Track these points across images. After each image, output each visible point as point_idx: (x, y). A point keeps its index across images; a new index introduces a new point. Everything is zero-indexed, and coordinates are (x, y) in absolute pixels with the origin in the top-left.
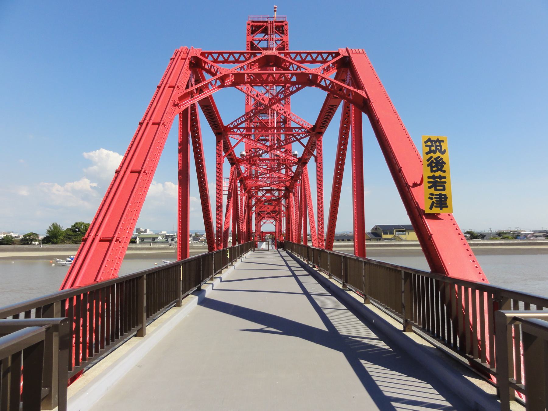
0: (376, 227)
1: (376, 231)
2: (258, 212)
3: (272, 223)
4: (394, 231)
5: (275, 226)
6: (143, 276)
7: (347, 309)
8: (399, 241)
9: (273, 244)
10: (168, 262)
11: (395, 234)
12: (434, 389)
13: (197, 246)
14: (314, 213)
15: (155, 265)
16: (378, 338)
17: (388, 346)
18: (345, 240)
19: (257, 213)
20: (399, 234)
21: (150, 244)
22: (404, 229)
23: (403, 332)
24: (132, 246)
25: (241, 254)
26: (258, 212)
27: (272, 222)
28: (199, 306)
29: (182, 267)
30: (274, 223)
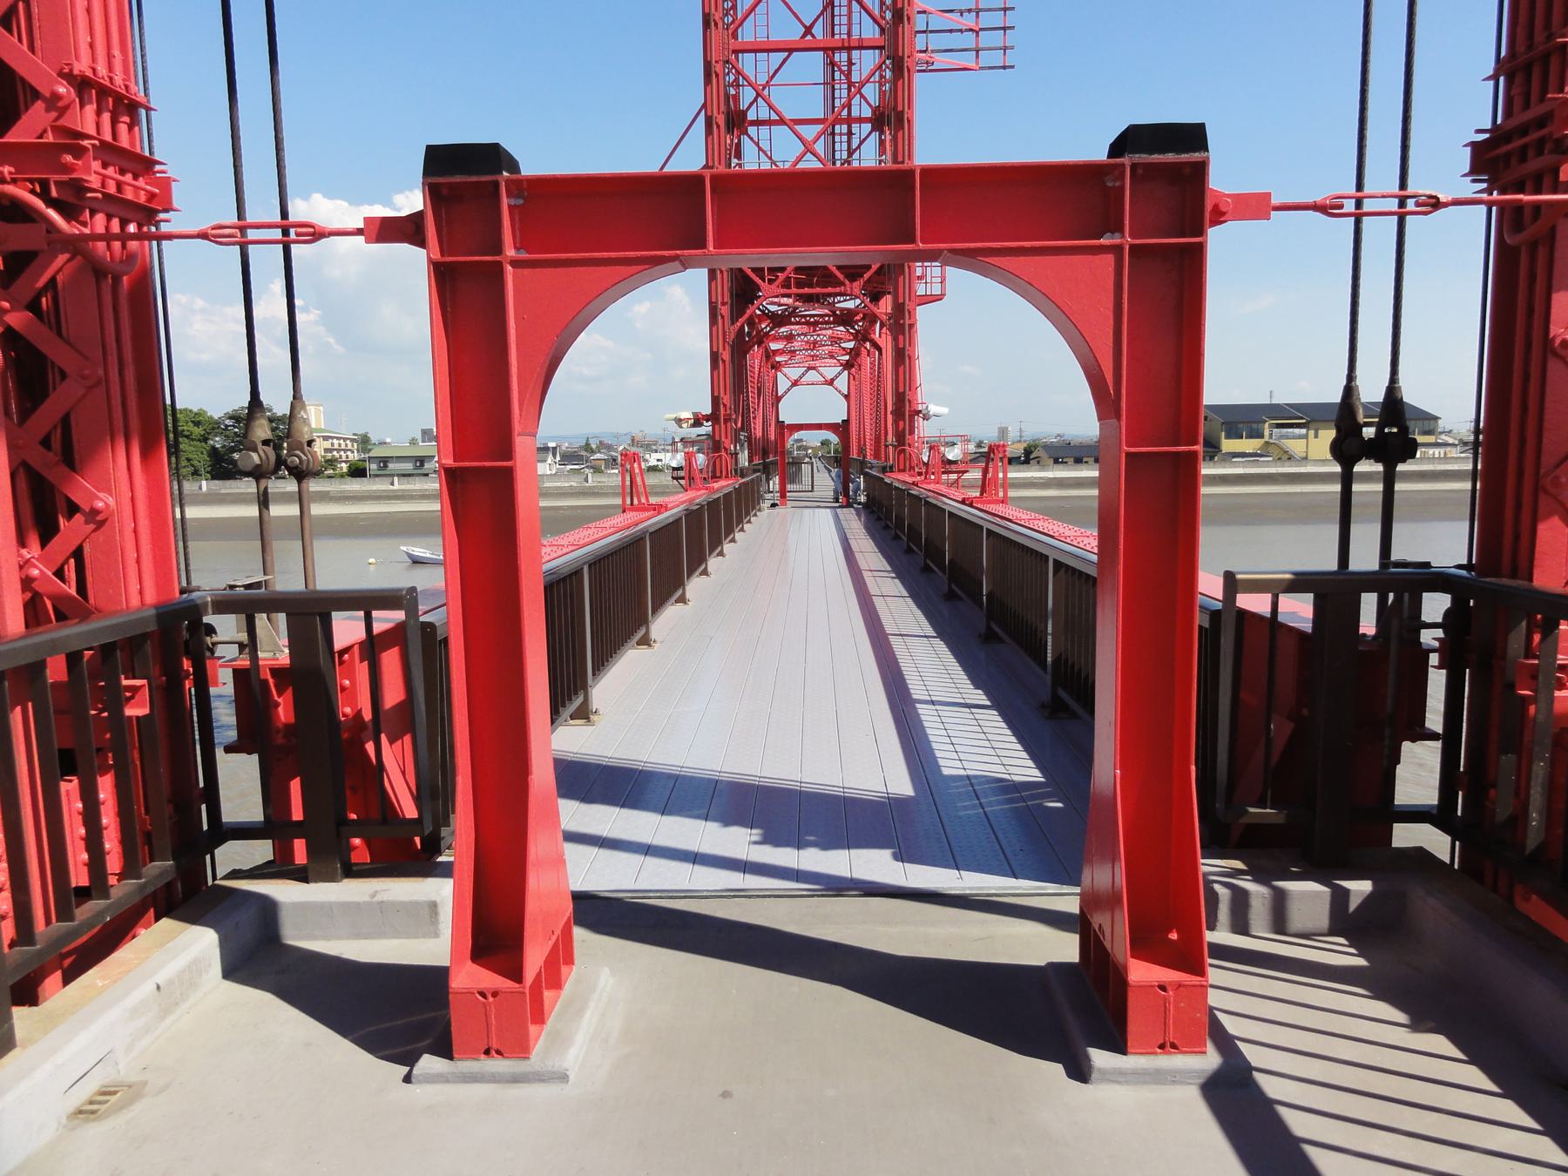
3: (831, 382)
4: (1267, 425)
5: (847, 397)
6: (582, 569)
8: (1279, 463)
9: (849, 505)
11: (1267, 438)
13: (559, 484)
15: (370, 564)
18: (1085, 460)
20: (1282, 437)
21: (390, 479)
22: (1302, 418)
24: (328, 489)
25: (748, 514)
27: (829, 377)
28: (228, 984)
30: (842, 382)
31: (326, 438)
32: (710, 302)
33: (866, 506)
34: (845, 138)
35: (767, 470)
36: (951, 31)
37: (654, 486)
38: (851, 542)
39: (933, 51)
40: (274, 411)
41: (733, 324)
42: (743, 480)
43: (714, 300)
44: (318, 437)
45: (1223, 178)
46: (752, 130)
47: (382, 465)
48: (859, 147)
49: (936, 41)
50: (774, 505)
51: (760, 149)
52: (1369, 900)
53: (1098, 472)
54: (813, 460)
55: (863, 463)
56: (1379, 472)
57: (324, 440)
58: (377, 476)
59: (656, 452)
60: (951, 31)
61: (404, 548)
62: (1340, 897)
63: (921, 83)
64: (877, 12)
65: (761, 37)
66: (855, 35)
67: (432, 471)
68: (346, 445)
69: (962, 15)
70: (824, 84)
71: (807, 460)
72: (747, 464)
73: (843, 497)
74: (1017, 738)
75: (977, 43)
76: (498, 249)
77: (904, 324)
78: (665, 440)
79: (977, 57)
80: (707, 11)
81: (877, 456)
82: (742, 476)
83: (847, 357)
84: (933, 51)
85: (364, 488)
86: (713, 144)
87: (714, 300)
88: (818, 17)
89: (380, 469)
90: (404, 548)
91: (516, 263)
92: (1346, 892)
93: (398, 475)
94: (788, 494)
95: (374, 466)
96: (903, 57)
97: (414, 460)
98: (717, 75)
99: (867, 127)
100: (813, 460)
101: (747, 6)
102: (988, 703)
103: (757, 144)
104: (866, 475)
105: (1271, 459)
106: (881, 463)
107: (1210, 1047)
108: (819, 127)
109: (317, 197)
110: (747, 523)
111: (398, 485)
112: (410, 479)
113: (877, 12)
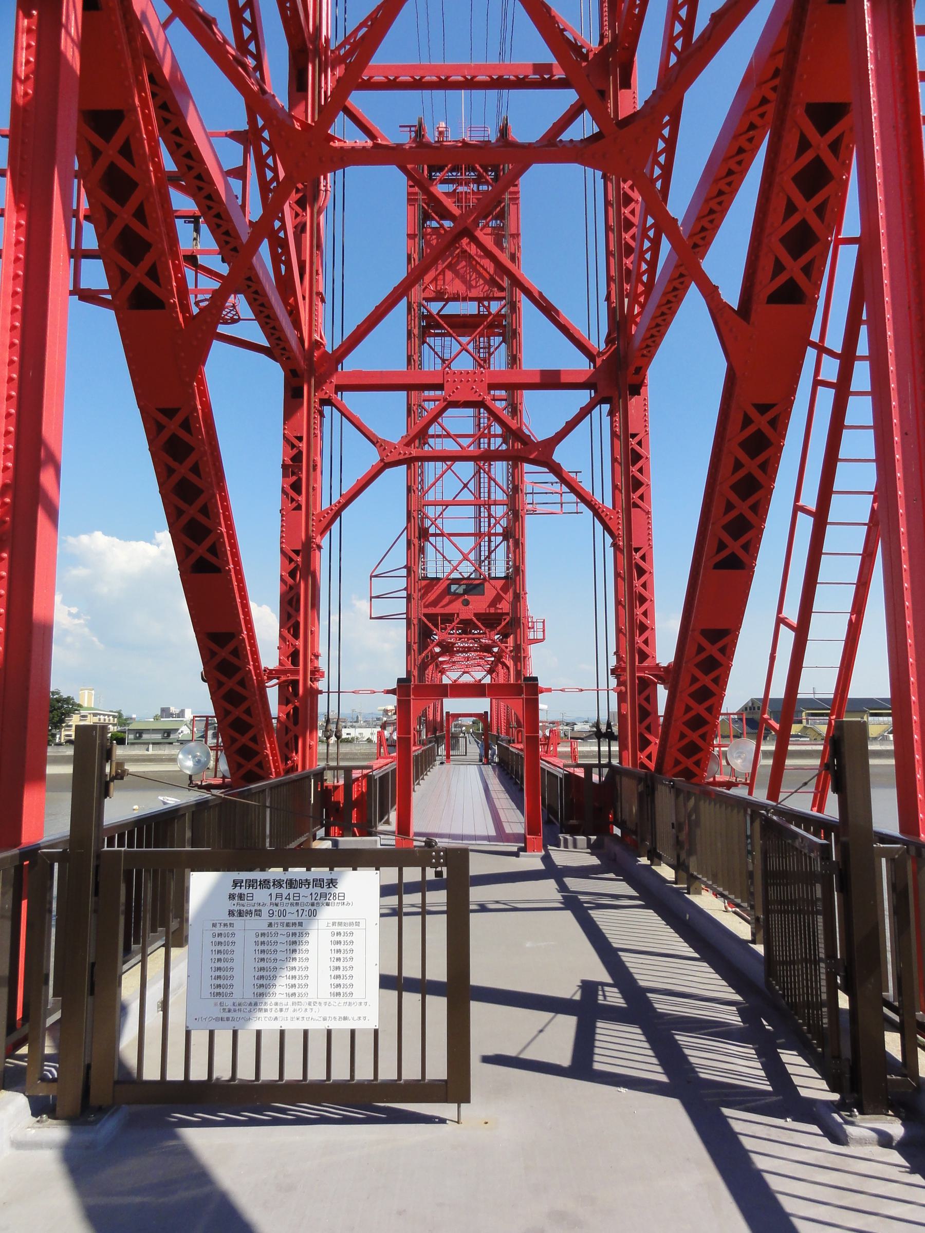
0: (753, 704)
1: (753, 713)
2: (420, 620)
4: (804, 714)
7: (697, 955)
9: (488, 763)
10: (172, 800)
12: (810, 1067)
14: (658, 626)
15: (134, 810)
16: (699, 956)
17: (717, 975)
19: (415, 622)
21: (146, 746)
23: (750, 945)
26: (420, 620)
29: (313, 780)
31: (95, 715)
32: (407, 642)
33: (498, 764)
34: (487, 520)
35: (438, 741)
36: (546, 493)
37: (346, 754)
38: (487, 780)
39: (536, 504)
40: (61, 694)
41: (420, 654)
42: (425, 748)
43: (409, 641)
44: (90, 714)
45: (541, 684)
46: (432, 539)
47: (138, 735)
48: (495, 550)
49: (538, 498)
50: (442, 763)
51: (436, 549)
52: (596, 840)
53: (870, 763)
54: (466, 735)
55: (498, 738)
56: (891, 750)
57: (94, 716)
58: (133, 744)
59: (345, 728)
60: (546, 493)
61: (161, 798)
62: (589, 840)
63: (529, 521)
64: (505, 488)
65: (439, 498)
66: (493, 497)
67: (176, 741)
68: (109, 720)
69: (552, 484)
70: (474, 518)
71: (462, 735)
72: (425, 737)
73: (485, 759)
74: (605, 936)
75: (561, 500)
76: (410, 697)
77: (520, 657)
78: (352, 718)
79: (562, 507)
80: (409, 484)
81: (507, 733)
82: (424, 744)
83: (493, 659)
84: (536, 504)
85: (125, 753)
86: (411, 554)
87: (409, 641)
88: (471, 479)
89: (136, 738)
90: (161, 798)
91: (413, 699)
92: (590, 839)
93: (153, 744)
94: (451, 757)
95: (131, 736)
96: (518, 510)
97: (163, 732)
98: (414, 518)
99: (500, 539)
100: (466, 735)
101: (431, 482)
102: (620, 953)
103: (435, 547)
104: (498, 745)
105: (808, 739)
106: (507, 738)
107: (543, 851)
108: (471, 440)
109: (98, 535)
110: (417, 784)
111: (152, 751)
112: (161, 746)
113: (505, 488)
